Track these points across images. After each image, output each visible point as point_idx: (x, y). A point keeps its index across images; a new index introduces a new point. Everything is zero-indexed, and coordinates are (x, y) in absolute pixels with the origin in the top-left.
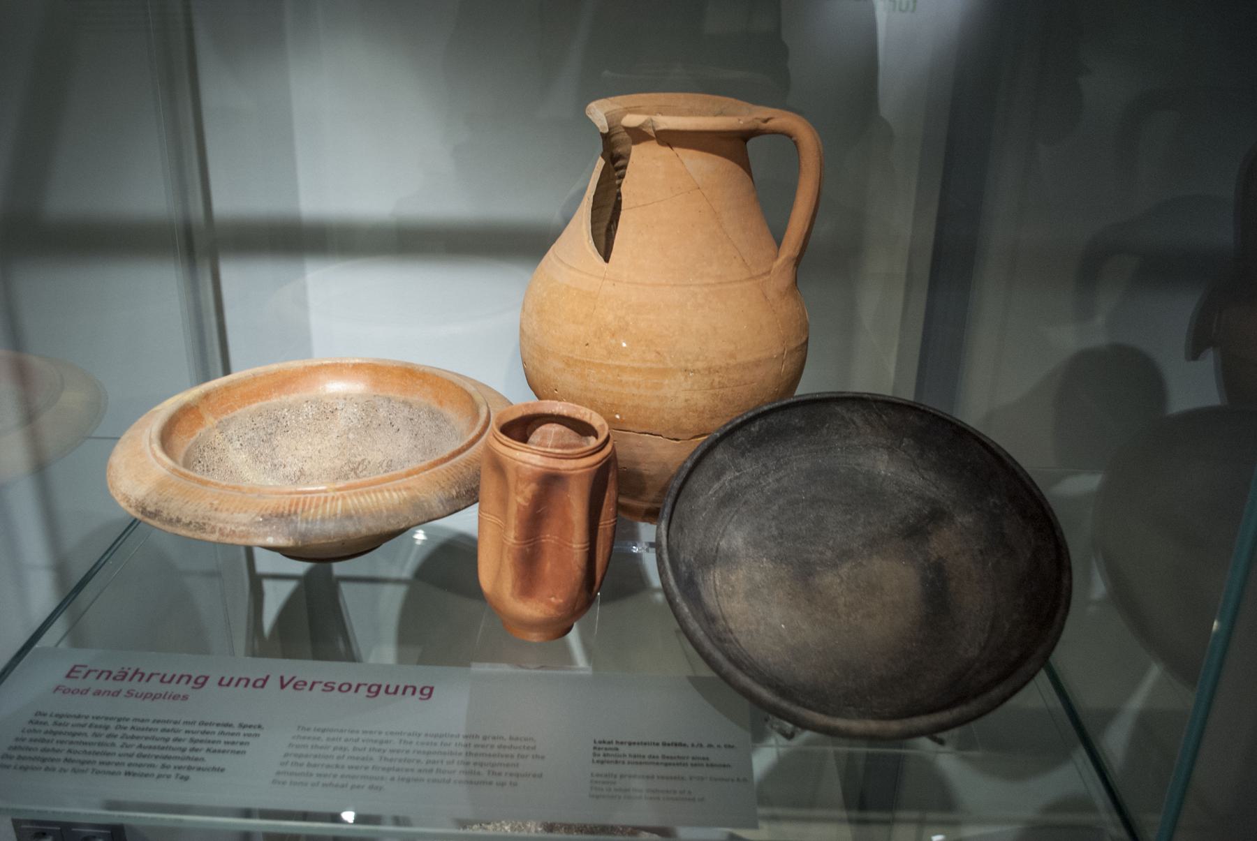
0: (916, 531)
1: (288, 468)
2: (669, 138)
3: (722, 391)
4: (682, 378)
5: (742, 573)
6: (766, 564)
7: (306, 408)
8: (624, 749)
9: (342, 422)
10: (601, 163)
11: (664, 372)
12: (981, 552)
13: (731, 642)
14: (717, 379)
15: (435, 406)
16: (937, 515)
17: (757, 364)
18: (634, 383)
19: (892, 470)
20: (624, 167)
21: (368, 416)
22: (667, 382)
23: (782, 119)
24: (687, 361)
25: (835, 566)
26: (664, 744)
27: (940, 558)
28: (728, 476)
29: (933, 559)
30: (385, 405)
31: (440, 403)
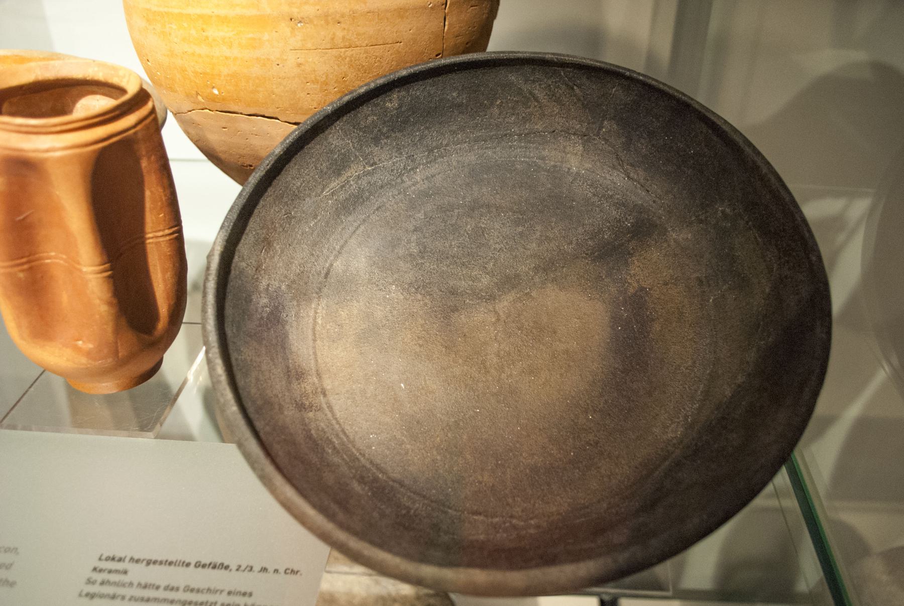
0: (613, 248)
3: (349, 52)
4: (288, 31)
5: (357, 307)
6: (395, 293)
8: (138, 573)
12: (700, 280)
13: (320, 409)
14: (340, 34)
16: (642, 229)
19: (588, 166)
25: (492, 298)
26: (198, 565)
27: (642, 289)
28: (354, 171)
29: (631, 290)
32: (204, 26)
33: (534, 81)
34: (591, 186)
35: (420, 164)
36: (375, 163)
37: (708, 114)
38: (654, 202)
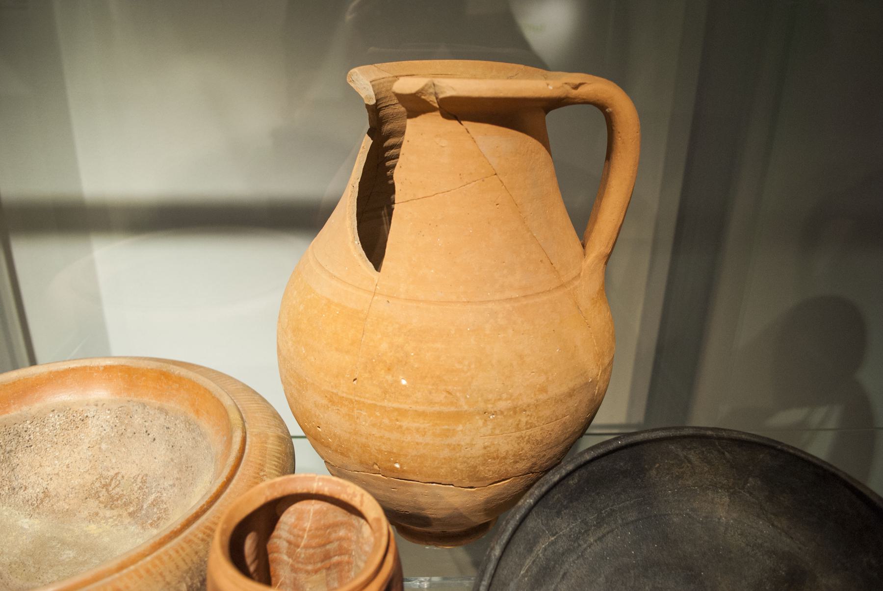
1: (30, 490)
2: (459, 110)
3: (529, 432)
4: (481, 423)
7: (53, 418)
9: (94, 431)
10: (367, 142)
11: (458, 416)
14: (524, 420)
15: (192, 416)
17: (571, 394)
18: (418, 430)
19: (735, 515)
20: (399, 146)
21: (122, 423)
22: (460, 427)
23: (596, 87)
24: (487, 401)
30: (140, 411)
31: (197, 412)
32: (399, 418)
33: (690, 449)
34: (741, 534)
36: (557, 533)
37: (855, 485)
38: (800, 549)
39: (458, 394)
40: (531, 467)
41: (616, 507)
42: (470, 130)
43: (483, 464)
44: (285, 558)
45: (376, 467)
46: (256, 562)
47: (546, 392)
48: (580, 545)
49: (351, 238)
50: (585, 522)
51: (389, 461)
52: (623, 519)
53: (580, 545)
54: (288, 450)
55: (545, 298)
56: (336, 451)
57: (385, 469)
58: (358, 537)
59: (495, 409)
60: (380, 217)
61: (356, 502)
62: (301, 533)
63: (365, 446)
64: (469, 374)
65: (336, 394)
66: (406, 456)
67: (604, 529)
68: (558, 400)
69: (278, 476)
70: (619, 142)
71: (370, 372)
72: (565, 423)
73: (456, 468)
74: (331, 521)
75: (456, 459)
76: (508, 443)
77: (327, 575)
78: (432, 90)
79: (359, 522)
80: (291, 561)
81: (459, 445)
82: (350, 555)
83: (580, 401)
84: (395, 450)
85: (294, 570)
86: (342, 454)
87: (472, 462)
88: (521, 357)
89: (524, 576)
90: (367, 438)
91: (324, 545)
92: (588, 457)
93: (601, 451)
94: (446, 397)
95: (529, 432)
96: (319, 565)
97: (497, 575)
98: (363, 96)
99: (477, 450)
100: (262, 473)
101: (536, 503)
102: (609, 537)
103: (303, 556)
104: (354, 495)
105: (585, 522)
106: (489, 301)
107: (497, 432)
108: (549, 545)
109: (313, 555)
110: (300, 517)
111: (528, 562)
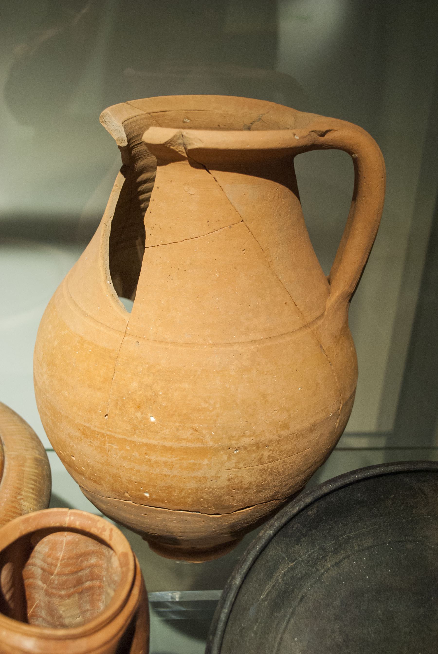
2: (205, 160)
3: (271, 465)
4: (225, 457)
10: (120, 180)
11: (204, 452)
14: (266, 454)
17: (312, 429)
18: (165, 463)
20: (153, 180)
22: (206, 462)
23: (344, 131)
24: (231, 438)
28: (282, 570)
32: (148, 452)
33: (424, 482)
35: (329, 552)
36: (296, 559)
39: (204, 432)
40: (274, 495)
41: (352, 534)
42: (217, 179)
43: (228, 494)
44: (40, 583)
45: (127, 495)
46: (12, 590)
47: (288, 429)
48: (317, 570)
49: (103, 278)
50: (322, 548)
51: (139, 490)
52: (359, 546)
53: (317, 570)
54: (45, 473)
55: (288, 339)
56: (90, 479)
57: (136, 497)
58: (108, 566)
59: (239, 445)
60: (135, 246)
61: (105, 536)
62: (54, 562)
63: (116, 477)
64: (214, 412)
65: (89, 428)
66: (155, 486)
67: (341, 555)
68: (299, 435)
69: (35, 510)
70: (364, 187)
71: (120, 409)
72: (306, 455)
73: (202, 498)
74: (83, 551)
75: (202, 490)
76: (251, 476)
77: (80, 599)
78: (180, 141)
79: (109, 553)
80: (45, 586)
81: (204, 477)
82: (101, 580)
83: (321, 435)
84: (144, 481)
85: (48, 594)
86: (95, 481)
87: (217, 493)
88: (264, 396)
89: (264, 600)
90: (118, 469)
91: (77, 572)
92: (325, 490)
93: (338, 484)
94: (192, 434)
95: (271, 465)
96: (72, 590)
97: (237, 601)
98: (115, 138)
99: (222, 482)
100: (19, 497)
101: (275, 535)
102: (346, 562)
103: (56, 582)
104: (104, 529)
105: (322, 548)
106: (234, 343)
107: (241, 465)
108: (288, 571)
109: (66, 581)
110: (54, 547)
111: (268, 587)
